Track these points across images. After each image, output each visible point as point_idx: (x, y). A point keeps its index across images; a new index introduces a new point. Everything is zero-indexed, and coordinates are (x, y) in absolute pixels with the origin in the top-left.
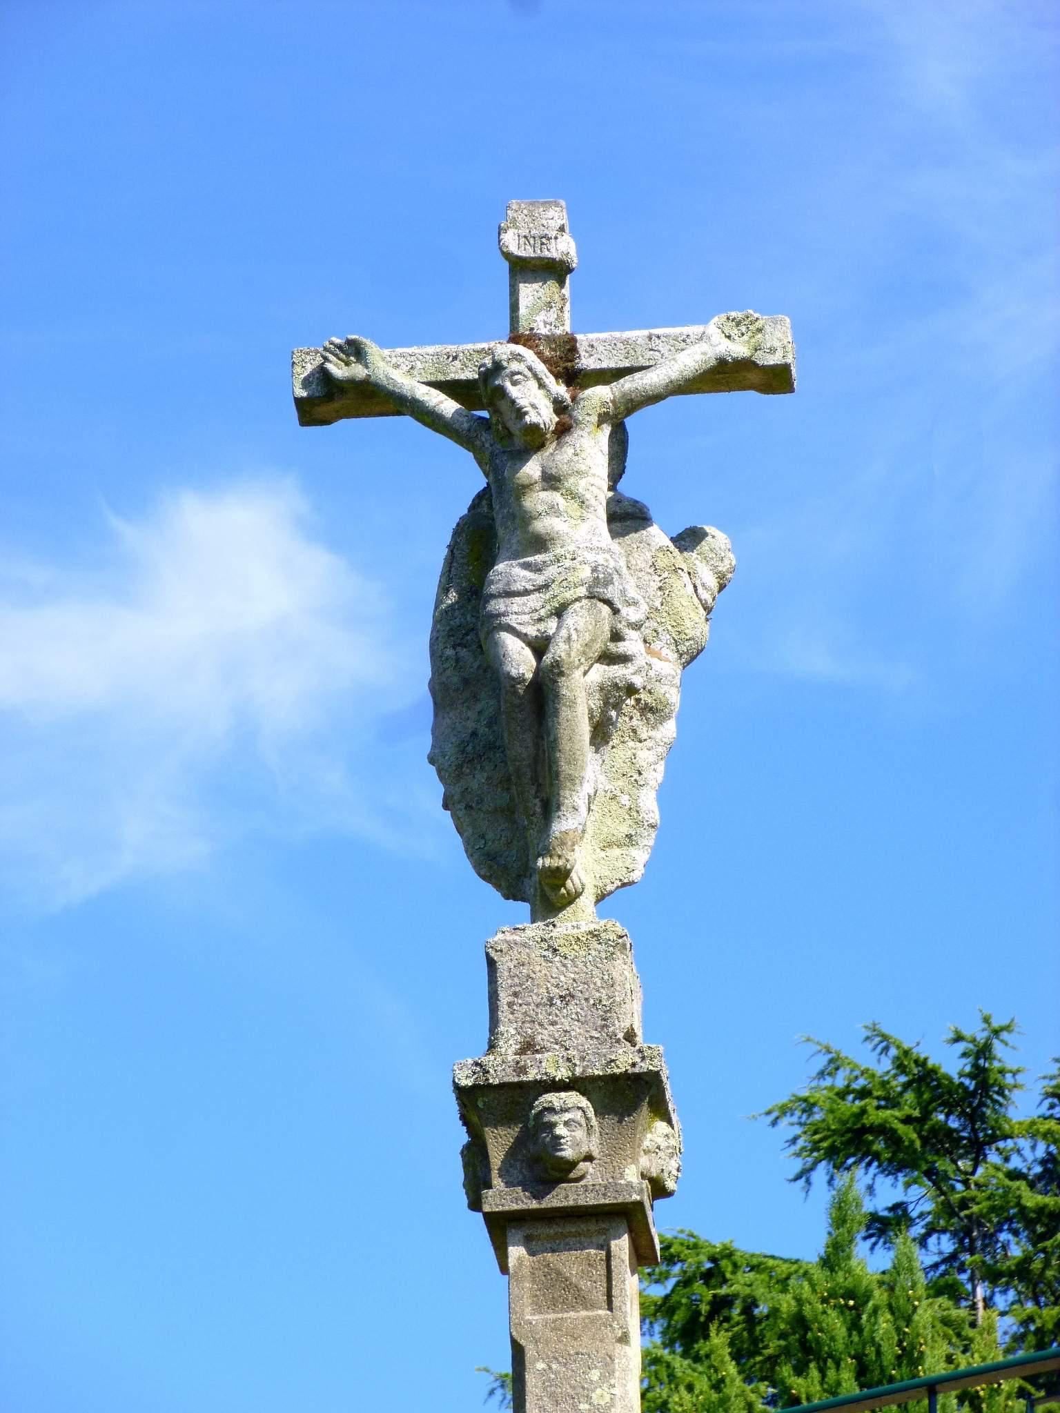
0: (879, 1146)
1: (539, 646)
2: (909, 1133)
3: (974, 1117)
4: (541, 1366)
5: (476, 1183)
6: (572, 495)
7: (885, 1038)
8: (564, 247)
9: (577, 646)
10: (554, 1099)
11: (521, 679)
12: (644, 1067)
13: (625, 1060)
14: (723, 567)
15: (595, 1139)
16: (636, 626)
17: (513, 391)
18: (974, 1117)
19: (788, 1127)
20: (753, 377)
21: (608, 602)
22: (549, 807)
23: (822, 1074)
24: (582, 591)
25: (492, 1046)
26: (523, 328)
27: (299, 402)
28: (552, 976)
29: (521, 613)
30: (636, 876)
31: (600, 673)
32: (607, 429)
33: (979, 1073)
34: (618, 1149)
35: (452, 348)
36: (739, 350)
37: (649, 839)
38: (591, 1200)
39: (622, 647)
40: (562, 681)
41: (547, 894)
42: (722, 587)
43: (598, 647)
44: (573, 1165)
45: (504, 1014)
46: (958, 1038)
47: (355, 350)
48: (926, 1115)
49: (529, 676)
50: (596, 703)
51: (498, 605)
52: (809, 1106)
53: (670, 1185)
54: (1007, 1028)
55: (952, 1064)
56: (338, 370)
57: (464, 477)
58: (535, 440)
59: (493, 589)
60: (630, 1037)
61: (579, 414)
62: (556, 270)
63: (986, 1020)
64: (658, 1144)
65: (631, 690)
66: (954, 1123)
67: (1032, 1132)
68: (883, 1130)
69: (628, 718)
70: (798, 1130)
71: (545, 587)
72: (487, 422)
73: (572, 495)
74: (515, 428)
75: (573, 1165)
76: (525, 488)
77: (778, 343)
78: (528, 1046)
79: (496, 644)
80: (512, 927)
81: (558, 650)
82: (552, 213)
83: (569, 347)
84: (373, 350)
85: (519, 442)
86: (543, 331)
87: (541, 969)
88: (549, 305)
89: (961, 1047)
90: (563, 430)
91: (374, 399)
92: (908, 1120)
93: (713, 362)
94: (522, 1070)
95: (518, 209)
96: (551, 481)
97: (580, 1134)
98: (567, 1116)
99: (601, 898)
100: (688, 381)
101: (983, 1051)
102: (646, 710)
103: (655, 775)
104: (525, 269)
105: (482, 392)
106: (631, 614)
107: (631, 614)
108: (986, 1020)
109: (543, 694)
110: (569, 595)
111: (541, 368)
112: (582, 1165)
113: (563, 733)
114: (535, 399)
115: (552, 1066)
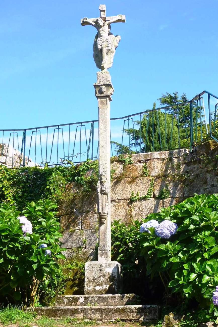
0: (167, 102)
1: (101, 46)
2: (169, 101)
3: (175, 100)
4: (101, 109)
5: (96, 93)
6: (104, 32)
7: (168, 93)
8: (105, 9)
9: (104, 45)
10: (102, 86)
11: (99, 49)
12: (110, 83)
13: (108, 83)
14: (120, 39)
15: (105, 90)
16: (110, 44)
17: (99, 22)
18: (175, 100)
19: (160, 101)
20: (122, 21)
21: (107, 42)
22: (102, 60)
23: (163, 96)
24: (105, 41)
25: (97, 82)
26: (101, 17)
27: (81, 24)
28: (102, 76)
29: (99, 43)
30: (111, 67)
31: (107, 48)
32: (108, 26)
33: (175, 96)
34: (108, 90)
35: (95, 19)
36: (120, 18)
37: (112, 64)
38: (105, 95)
39: (108, 46)
40: (103, 49)
41: (102, 68)
42: (120, 41)
43: (106, 46)
44: (103, 92)
45: (98, 79)
46: (174, 93)
47: (86, 19)
48: (171, 100)
49: (100, 49)
50: (106, 51)
51: (98, 42)
52: (161, 99)
53: (112, 94)
54: (178, 93)
55: (173, 96)
56: (85, 21)
57: (95, 31)
58: (101, 26)
59: (97, 41)
60: (109, 81)
61: (105, 24)
62: (104, 11)
63: (176, 92)
64: (111, 91)
65: (109, 50)
66: (173, 100)
67: (180, 101)
68: (167, 101)
69: (109, 53)
70: (160, 101)
71: (102, 40)
72: (97, 25)
73: (104, 32)
74: (99, 26)
75: (103, 92)
76: (101, 31)
77: (124, 18)
78: (100, 82)
79: (97, 45)
80: (99, 72)
81: (103, 46)
82: (104, 5)
83: (105, 18)
84: (87, 18)
85: (100, 27)
86: (103, 17)
87: (101, 75)
88: (103, 14)
89: (174, 94)
90: (104, 26)
91: (88, 23)
92: (169, 100)
93: (117, 19)
94: (99, 84)
95: (101, 5)
96: (103, 30)
97: (104, 89)
98: (103, 88)
99: (107, 69)
100: (115, 21)
101: (176, 94)
102: (112, 52)
103: (113, 58)
104: (101, 11)
105: (97, 22)
106: (109, 43)
107: (109, 43)
108: (176, 92)
109: (101, 50)
110: (104, 41)
111: (102, 20)
112: (104, 92)
113: (103, 54)
114: (101, 23)
115: (102, 83)
